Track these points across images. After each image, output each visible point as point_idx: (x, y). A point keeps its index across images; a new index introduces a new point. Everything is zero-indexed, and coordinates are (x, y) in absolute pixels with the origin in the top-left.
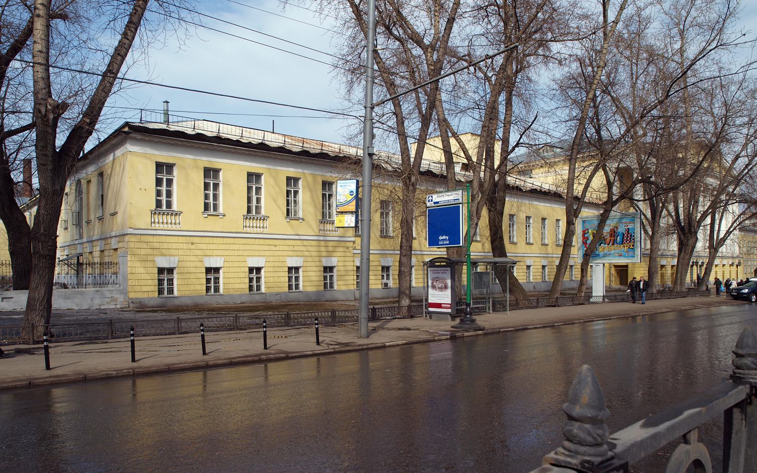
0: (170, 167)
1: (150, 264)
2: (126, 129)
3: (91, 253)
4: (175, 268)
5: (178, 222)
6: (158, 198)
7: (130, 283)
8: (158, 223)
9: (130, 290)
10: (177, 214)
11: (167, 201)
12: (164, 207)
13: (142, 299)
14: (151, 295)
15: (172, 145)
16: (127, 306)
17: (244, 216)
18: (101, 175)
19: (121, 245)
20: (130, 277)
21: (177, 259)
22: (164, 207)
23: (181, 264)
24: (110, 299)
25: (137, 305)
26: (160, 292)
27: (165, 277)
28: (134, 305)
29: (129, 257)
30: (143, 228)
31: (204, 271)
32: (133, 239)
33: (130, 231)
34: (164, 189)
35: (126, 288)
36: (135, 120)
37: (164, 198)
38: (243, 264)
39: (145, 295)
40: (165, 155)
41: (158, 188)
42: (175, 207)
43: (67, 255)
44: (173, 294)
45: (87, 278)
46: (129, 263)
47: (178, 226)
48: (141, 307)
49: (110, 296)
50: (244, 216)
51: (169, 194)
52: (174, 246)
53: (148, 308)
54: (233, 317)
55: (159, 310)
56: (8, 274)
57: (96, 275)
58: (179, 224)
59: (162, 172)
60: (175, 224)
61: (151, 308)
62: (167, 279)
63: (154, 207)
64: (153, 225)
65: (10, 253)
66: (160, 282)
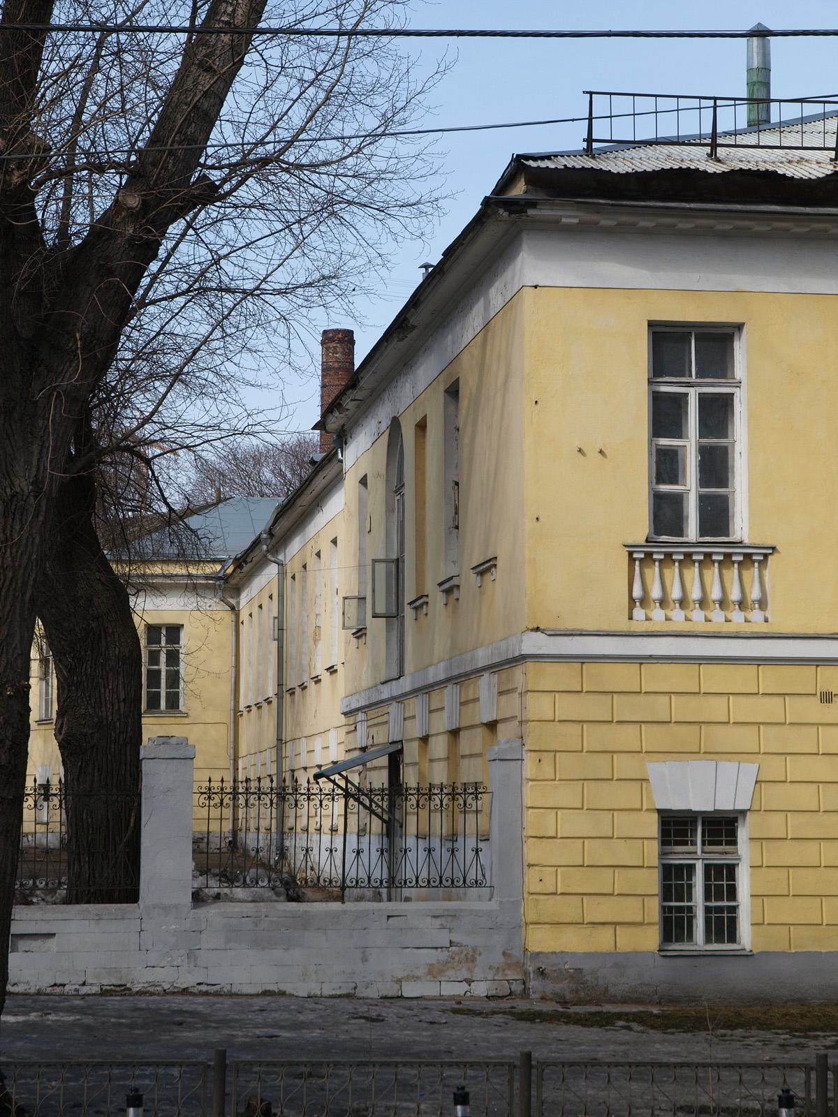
0: (716, 342)
1: (627, 796)
2: (519, 190)
3: (425, 740)
4: (743, 813)
5: (755, 594)
6: (665, 488)
7: (532, 881)
8: (663, 602)
9: (531, 917)
10: (756, 557)
11: (703, 499)
12: (692, 530)
13: (588, 955)
14: (628, 941)
15: (724, 237)
16: (518, 988)
17: (631, 550)
18: (453, 392)
19: (510, 706)
20: (532, 852)
21: (749, 771)
22: (692, 530)
23: (774, 797)
24: (443, 955)
25: (563, 987)
26: (674, 925)
27: (697, 855)
28: (550, 987)
29: (529, 760)
30: (591, 627)
31: (651, 826)
32: (552, 676)
33: (533, 644)
34: (690, 444)
35: (516, 904)
36: (561, 142)
37: (690, 486)
38: (627, 796)
39: (603, 941)
40: (692, 287)
41: (664, 442)
42: (742, 527)
43: (363, 749)
44: (733, 938)
45: (350, 856)
46: (528, 789)
47: (756, 615)
48: (582, 1000)
49: (443, 938)
50: (631, 550)
51: (716, 467)
52: (742, 709)
53: (613, 1000)
54: (808, 1069)
55: (619, 1016)
56: (215, 827)
57: (436, 843)
58: (762, 604)
59: (680, 369)
60: (742, 604)
61: (624, 1001)
62: (707, 868)
63: (640, 529)
64: (639, 613)
65: (61, 747)
66: (674, 880)
